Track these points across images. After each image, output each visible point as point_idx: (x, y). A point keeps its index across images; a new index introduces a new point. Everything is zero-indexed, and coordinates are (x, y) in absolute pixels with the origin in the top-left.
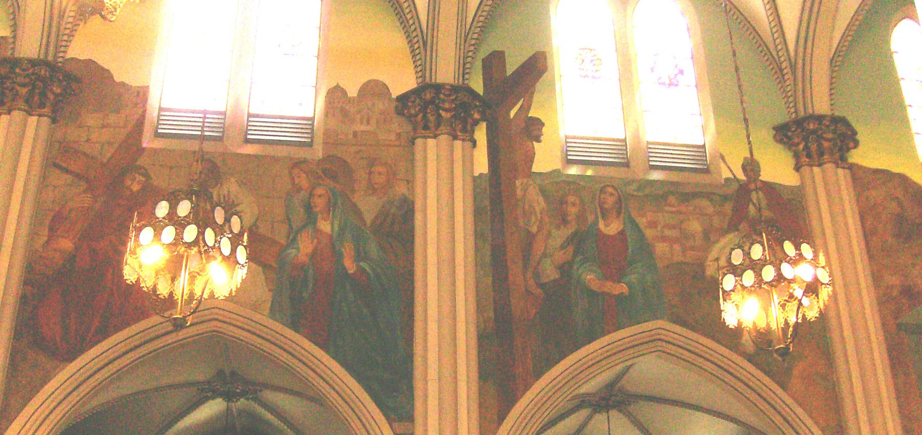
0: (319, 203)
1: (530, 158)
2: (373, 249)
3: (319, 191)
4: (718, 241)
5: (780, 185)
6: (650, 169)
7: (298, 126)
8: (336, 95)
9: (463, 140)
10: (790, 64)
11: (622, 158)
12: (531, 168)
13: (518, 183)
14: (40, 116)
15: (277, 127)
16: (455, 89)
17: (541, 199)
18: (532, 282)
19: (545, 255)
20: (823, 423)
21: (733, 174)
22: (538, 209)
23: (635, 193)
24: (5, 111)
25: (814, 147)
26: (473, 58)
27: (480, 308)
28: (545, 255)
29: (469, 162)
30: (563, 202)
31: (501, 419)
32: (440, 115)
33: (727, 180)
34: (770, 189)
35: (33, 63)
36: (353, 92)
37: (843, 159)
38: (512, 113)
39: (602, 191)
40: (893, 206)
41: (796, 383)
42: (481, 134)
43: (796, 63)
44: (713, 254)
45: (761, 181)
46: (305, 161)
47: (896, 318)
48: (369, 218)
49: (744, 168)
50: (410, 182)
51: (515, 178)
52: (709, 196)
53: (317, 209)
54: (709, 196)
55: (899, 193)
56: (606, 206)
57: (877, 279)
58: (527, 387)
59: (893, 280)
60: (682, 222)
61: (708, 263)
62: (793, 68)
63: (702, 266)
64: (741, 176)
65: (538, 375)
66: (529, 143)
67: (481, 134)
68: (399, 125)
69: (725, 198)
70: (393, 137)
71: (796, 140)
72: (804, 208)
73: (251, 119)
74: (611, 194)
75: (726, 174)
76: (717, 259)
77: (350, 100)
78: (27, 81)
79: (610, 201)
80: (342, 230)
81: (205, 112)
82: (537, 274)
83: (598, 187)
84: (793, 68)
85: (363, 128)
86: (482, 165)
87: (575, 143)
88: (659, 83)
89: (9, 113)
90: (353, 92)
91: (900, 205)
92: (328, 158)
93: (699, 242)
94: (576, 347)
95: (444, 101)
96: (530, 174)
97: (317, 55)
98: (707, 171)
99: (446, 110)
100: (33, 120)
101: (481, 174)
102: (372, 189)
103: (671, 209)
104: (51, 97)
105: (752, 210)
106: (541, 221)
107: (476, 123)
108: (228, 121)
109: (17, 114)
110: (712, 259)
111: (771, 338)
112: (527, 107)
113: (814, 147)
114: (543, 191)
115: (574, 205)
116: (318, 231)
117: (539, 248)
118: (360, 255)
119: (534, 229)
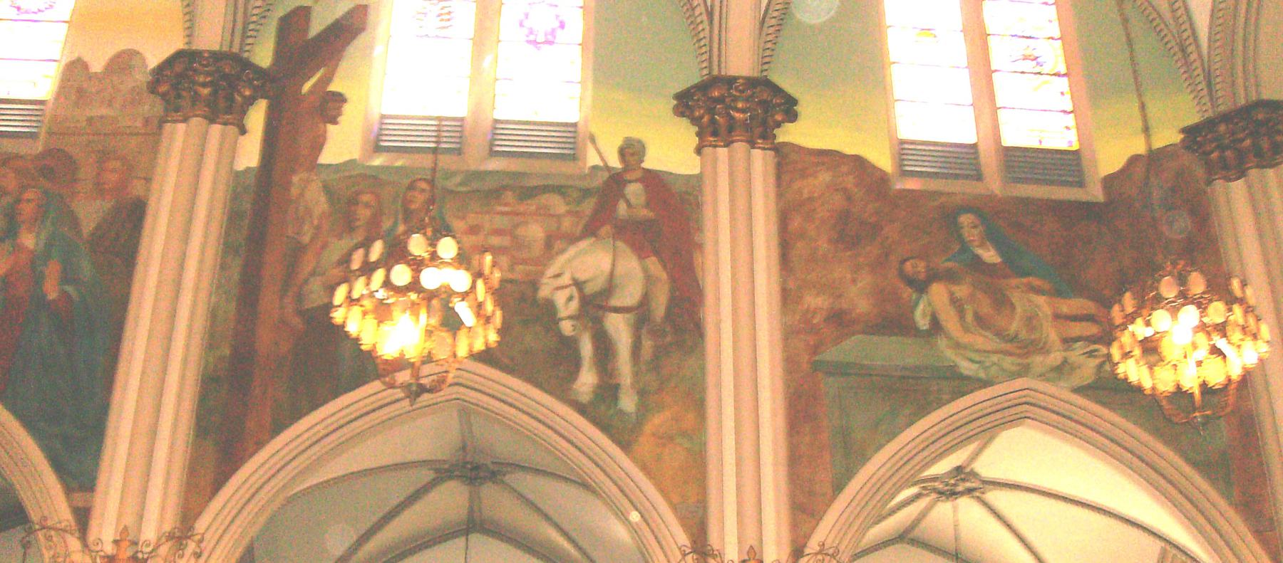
0: (27, 209)
1: (318, 145)
2: (86, 268)
3: (30, 195)
4: (562, 251)
5: (666, 172)
6: (491, 156)
7: (24, 113)
8: (75, 70)
9: (764, 149)
10: (707, 10)
11: (571, 149)
12: (317, 159)
13: (295, 179)
14: (225, 124)
15: (395, 130)
16: (752, 83)
17: (323, 199)
18: (290, 309)
19: (313, 274)
20: (676, 499)
21: (602, 158)
22: (317, 212)
23: (461, 189)
24: (180, 118)
25: (1265, 144)
26: (773, 50)
27: (211, 343)
28: (313, 274)
29: (232, 152)
30: (353, 201)
31: (217, 486)
32: (732, 118)
33: (595, 168)
34: (654, 181)
35: (217, 56)
36: (97, 66)
37: (767, 135)
38: (307, 87)
39: (411, 187)
40: (838, 200)
41: (645, 445)
42: (257, 117)
43: (712, 9)
44: (551, 271)
45: (643, 169)
46: (18, 157)
47: (815, 353)
48: (88, 226)
49: (622, 152)
50: (148, 180)
51: (294, 172)
52: (559, 190)
53: (358, 223)
54: (559, 190)
55: (850, 181)
56: (413, 207)
57: (787, 297)
58: (260, 445)
59: (816, 301)
60: (517, 226)
61: (545, 281)
62: (710, 14)
63: (534, 285)
64: (615, 162)
65: (277, 429)
66: (321, 125)
67: (257, 117)
68: (152, 107)
69: (586, 193)
70: (139, 124)
71: (1241, 135)
72: (699, 205)
73: (498, 126)
74: (423, 190)
75: (593, 159)
76: (558, 276)
77: (91, 77)
78: (209, 79)
79: (419, 200)
80: (49, 245)
81: (440, 119)
82: (300, 297)
83: (406, 182)
84: (710, 14)
85: (104, 111)
86: (249, 154)
87: (394, 124)
88: (529, 42)
89: (185, 120)
90: (97, 66)
91: (849, 198)
92: (48, 153)
93: (537, 250)
94: (335, 394)
95: (735, 99)
96: (314, 166)
97: (994, 75)
98: (574, 158)
99: (739, 110)
100: (216, 129)
101: (248, 170)
102: (100, 189)
103: (506, 209)
104: (239, 99)
105: (622, 208)
106: (318, 228)
107: (250, 101)
108: (467, 127)
109: (1254, 173)
110: (548, 276)
111: (618, 382)
112: (328, 79)
113: (1265, 144)
114: (327, 189)
115: (367, 206)
116: (18, 248)
117: (307, 265)
118: (68, 276)
119: (306, 239)
